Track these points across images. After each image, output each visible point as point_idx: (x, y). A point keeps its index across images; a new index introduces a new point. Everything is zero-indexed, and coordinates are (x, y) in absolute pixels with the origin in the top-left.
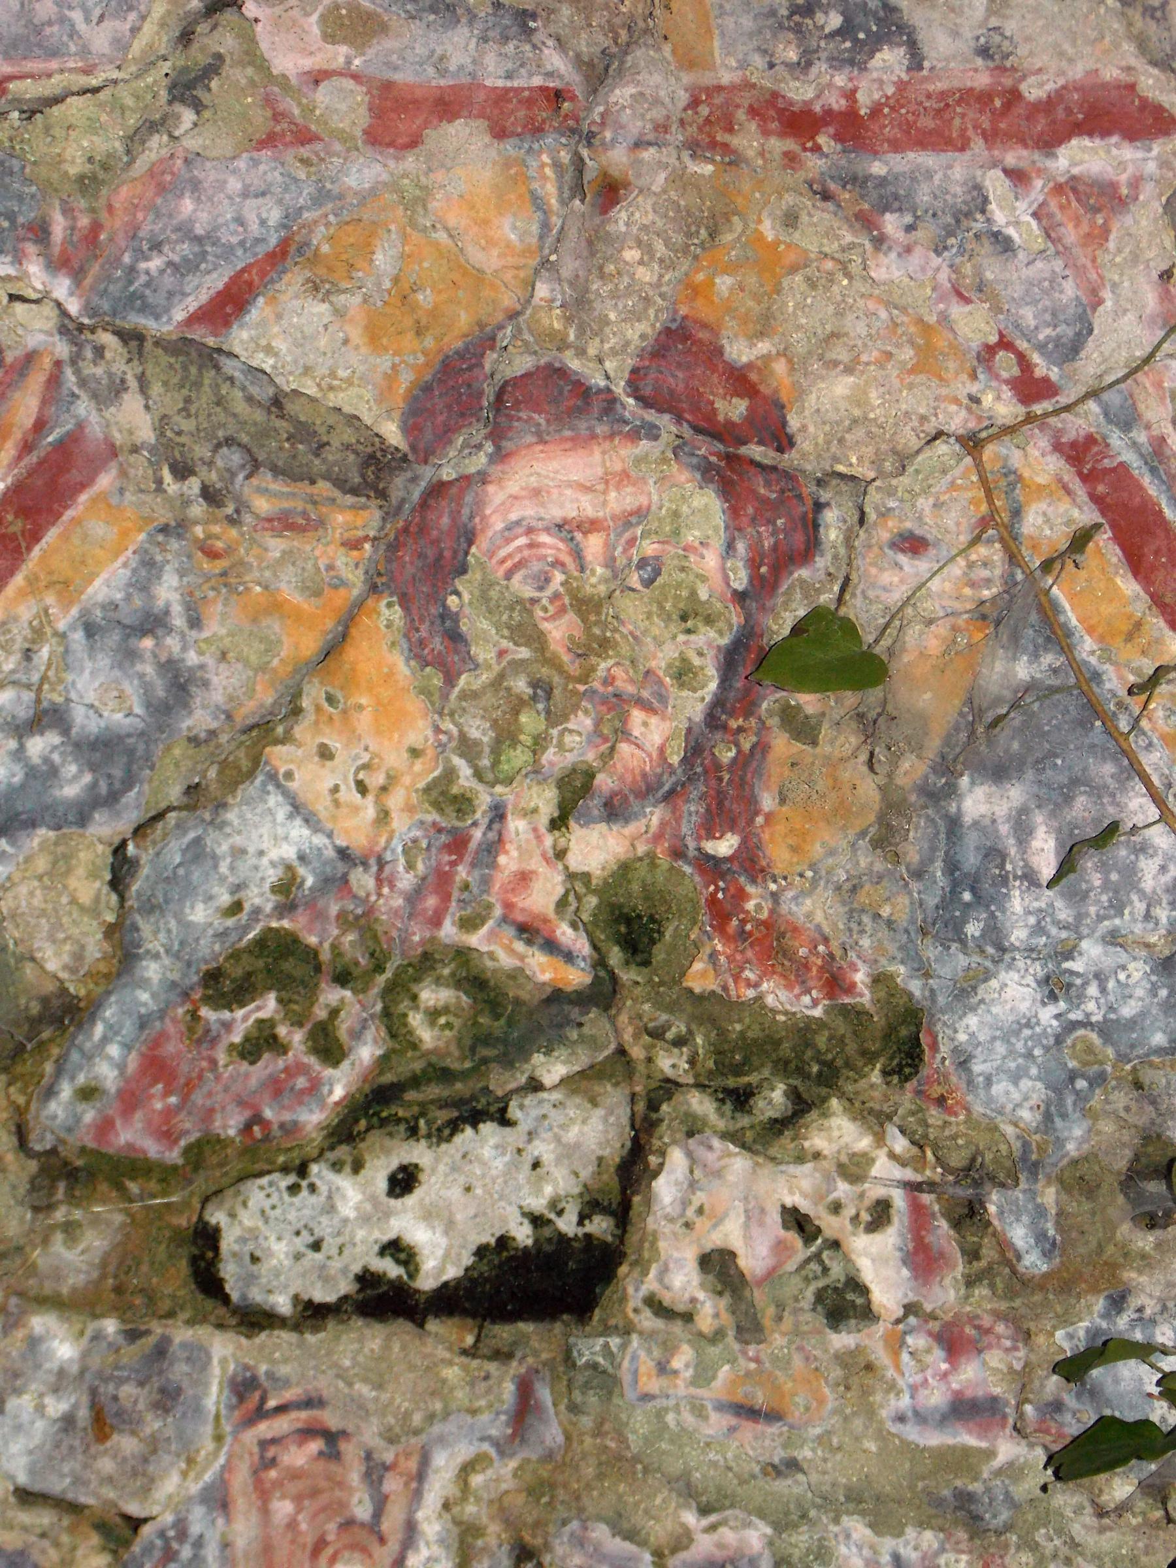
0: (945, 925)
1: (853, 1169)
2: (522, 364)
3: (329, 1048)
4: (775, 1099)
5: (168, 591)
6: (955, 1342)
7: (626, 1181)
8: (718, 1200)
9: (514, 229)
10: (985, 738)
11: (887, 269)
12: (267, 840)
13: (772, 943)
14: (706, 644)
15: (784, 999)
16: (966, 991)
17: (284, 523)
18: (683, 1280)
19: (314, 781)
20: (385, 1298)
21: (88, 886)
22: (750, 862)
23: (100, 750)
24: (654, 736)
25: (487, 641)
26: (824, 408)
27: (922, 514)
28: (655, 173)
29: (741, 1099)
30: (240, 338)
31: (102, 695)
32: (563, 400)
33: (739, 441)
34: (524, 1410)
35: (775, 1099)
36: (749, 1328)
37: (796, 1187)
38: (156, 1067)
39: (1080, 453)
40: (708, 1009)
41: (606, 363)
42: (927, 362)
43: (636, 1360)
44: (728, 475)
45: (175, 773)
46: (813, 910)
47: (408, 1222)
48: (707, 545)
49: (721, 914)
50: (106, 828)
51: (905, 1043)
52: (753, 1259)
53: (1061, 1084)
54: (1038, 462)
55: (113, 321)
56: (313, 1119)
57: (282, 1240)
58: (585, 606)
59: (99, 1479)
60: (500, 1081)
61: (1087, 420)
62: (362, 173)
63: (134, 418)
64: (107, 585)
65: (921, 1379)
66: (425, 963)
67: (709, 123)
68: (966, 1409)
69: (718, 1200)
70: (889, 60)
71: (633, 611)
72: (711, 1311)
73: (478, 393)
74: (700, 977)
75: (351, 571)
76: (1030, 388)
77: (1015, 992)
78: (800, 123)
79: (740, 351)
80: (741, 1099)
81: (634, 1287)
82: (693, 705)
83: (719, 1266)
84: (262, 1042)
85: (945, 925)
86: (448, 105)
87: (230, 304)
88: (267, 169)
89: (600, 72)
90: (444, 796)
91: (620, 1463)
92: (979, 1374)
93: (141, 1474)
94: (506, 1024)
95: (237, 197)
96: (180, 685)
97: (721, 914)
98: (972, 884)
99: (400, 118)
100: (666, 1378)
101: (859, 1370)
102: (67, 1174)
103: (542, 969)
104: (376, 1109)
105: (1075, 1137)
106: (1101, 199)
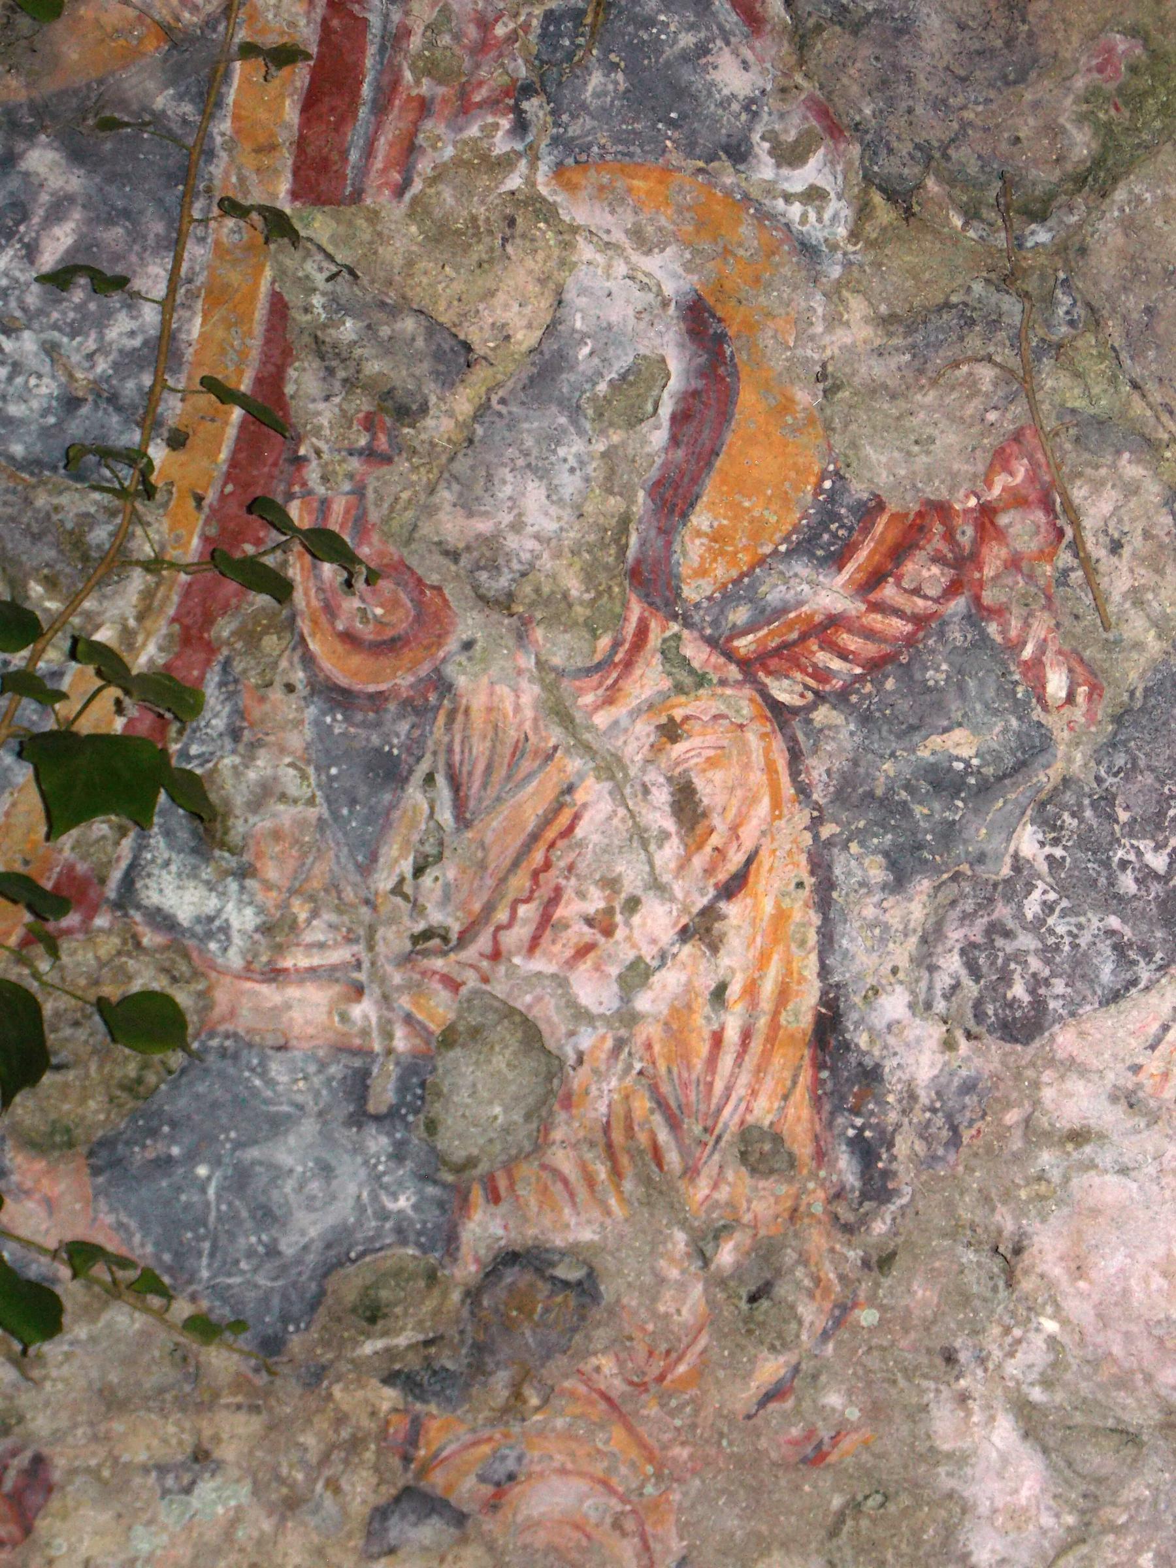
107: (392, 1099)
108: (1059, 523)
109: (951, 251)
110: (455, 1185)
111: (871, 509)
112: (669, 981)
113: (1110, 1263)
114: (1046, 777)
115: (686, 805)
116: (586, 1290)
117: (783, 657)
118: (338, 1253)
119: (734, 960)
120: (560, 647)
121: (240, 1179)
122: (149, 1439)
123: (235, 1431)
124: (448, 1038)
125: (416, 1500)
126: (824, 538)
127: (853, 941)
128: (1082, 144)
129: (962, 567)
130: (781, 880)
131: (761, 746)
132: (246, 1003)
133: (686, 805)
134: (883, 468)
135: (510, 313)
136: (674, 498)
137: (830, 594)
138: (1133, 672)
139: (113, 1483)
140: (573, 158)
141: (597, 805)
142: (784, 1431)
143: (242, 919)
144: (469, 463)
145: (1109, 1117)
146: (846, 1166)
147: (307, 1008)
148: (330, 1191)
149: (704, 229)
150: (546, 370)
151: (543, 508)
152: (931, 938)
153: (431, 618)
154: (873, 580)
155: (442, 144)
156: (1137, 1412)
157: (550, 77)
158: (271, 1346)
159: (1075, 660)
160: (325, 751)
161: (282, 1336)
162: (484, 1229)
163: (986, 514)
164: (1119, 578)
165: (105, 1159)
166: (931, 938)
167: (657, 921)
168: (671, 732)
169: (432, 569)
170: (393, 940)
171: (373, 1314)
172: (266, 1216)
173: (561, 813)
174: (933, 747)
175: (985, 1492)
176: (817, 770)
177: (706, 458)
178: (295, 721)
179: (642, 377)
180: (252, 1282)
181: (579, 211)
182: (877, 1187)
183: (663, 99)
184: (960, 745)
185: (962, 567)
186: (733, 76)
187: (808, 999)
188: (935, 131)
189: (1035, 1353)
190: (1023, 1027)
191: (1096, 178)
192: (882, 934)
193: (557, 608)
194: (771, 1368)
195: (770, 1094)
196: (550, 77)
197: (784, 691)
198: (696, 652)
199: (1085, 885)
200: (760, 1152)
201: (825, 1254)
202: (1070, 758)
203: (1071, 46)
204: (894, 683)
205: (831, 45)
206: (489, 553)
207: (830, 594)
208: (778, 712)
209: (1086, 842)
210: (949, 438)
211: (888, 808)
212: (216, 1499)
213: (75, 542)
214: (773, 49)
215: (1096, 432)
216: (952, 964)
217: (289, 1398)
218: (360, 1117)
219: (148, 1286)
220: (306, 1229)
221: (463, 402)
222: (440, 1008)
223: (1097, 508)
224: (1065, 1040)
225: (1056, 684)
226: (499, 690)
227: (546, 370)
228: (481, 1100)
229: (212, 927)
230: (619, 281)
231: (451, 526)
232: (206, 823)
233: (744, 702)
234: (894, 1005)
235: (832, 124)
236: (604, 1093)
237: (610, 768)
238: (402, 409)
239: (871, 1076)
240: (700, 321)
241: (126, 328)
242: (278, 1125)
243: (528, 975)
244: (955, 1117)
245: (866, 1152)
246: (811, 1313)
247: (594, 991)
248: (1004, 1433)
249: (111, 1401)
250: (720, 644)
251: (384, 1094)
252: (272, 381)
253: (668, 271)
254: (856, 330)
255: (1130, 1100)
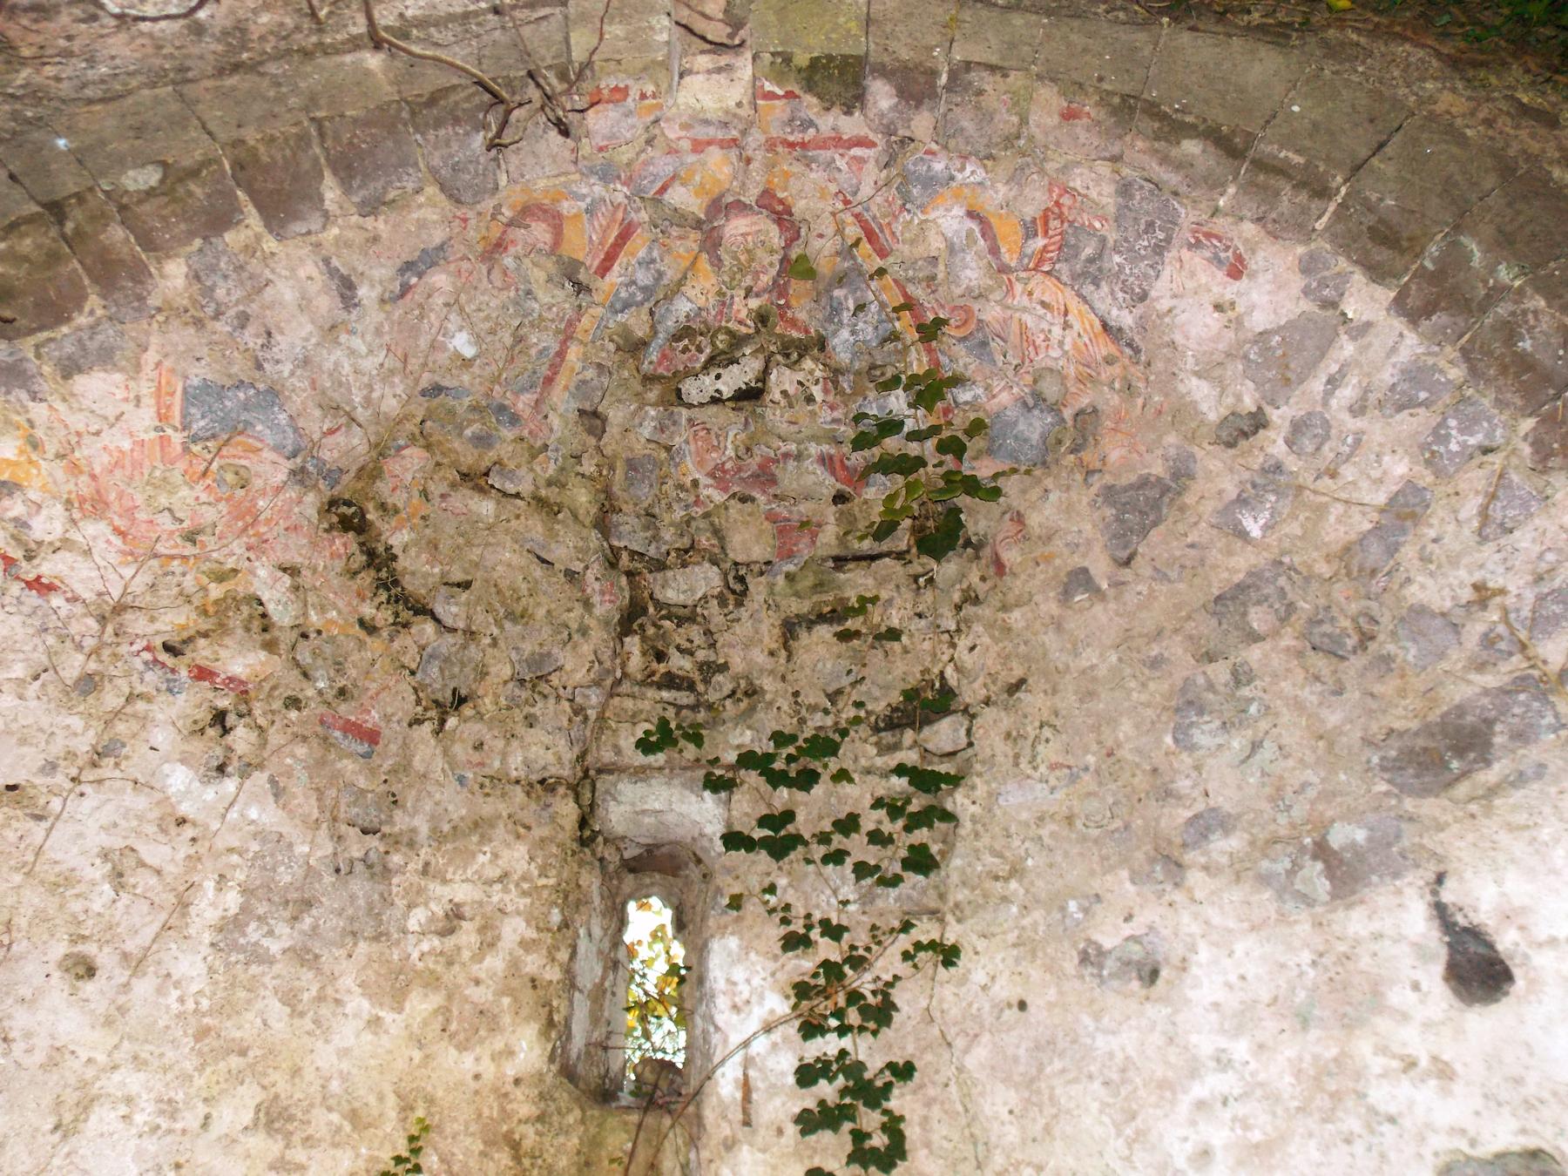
0: (830, 320)
1: (811, 372)
2: (730, 199)
3: (700, 350)
4: (795, 356)
5: (655, 254)
6: (832, 408)
7: (764, 376)
8: (783, 380)
9: (727, 170)
10: (840, 280)
11: (813, 175)
12: (682, 307)
13: (793, 323)
14: (777, 258)
15: (795, 334)
16: (835, 333)
17: (680, 238)
18: (777, 396)
19: (691, 293)
20: (716, 400)
21: (645, 317)
22: (788, 306)
23: (644, 289)
24: (766, 279)
25: (727, 260)
26: (799, 207)
27: (822, 229)
28: (759, 156)
29: (787, 356)
30: (666, 196)
31: (644, 278)
32: (740, 207)
33: (783, 216)
34: (746, 423)
35: (795, 356)
36: (791, 406)
37: (800, 376)
38: (664, 356)
39: (857, 216)
40: (781, 336)
41: (750, 198)
42: (822, 197)
43: (769, 412)
44: (779, 221)
45: (660, 294)
46: (802, 316)
47: (719, 385)
48: (775, 237)
49: (782, 317)
50: (647, 305)
51: (822, 343)
52: (791, 391)
53: (854, 354)
54: (850, 219)
55: (639, 193)
56: (698, 366)
57: (695, 389)
58: (748, 251)
59: (663, 439)
60: (738, 354)
61: (858, 210)
62: (691, 158)
63: (644, 216)
64: (642, 254)
65: (826, 415)
66: (719, 329)
67: (771, 145)
68: (834, 421)
69: (783, 380)
70: (812, 131)
71: (759, 253)
72: (783, 402)
73: (720, 207)
74: (778, 330)
75: (696, 247)
76: (846, 202)
77: (845, 334)
78: (792, 145)
79: (781, 195)
80: (787, 356)
81: (767, 398)
82: (774, 272)
83: (784, 393)
84: (685, 350)
85: (830, 320)
86: (709, 143)
87: (663, 189)
88: (669, 159)
89: (744, 133)
90: (720, 293)
91: (767, 432)
92: (837, 414)
93: (671, 438)
94: (737, 341)
95: (664, 166)
96: (660, 274)
97: (782, 317)
98: (836, 310)
99: (699, 146)
100: (775, 416)
101: (813, 414)
102: (649, 379)
103: (744, 330)
104: (711, 362)
105: (857, 365)
106: (861, 161)
107: (1036, 401)
108: (860, 751)
109: (1008, 161)
110: (1055, 409)
111: (1034, 221)
112: (1068, 340)
113: (1193, 332)
114: (1111, 243)
115: (1044, 304)
116: (1095, 411)
117: (1041, 261)
118: (1044, 438)
119: (1077, 326)
120: (997, 295)
121: (1016, 438)
122: (1035, 494)
123: (1049, 482)
124: (1035, 381)
125: (1090, 473)
126: (1030, 232)
127: (1097, 305)
128: (1015, 119)
129: (1061, 217)
130: (1074, 305)
131: (1050, 282)
132: (993, 406)
133: (1044, 304)
134: (1031, 211)
135: (936, 244)
136: (994, 251)
137: (1040, 242)
138: (1112, 210)
139: (1033, 506)
140: (923, 208)
141: (1029, 319)
142: (1150, 411)
143: (980, 391)
144: (952, 277)
145: (1174, 302)
146: (1128, 351)
147: (1004, 398)
148: (1034, 427)
149: (957, 196)
150: (951, 249)
151: (972, 273)
152: (1112, 293)
153: (967, 310)
154: (1046, 233)
155: (898, 228)
156: (1218, 357)
157: (906, 198)
158: (1044, 463)
159: (1098, 217)
160: (970, 350)
161: (1044, 459)
162: (1068, 414)
163: (1057, 204)
164: (1093, 194)
165: (990, 452)
166: (1112, 293)
167: (1057, 331)
168: (1030, 294)
169: (961, 302)
170: (1010, 373)
171: (1059, 442)
172: (1026, 440)
173: (1023, 328)
174: (1083, 256)
175: (1197, 396)
176: (1064, 278)
177: (994, 238)
178: (960, 350)
179: (970, 233)
180: (1032, 454)
181: (931, 216)
182: (1137, 351)
183: (929, 182)
184: (1089, 251)
185: (1061, 217)
186: (938, 166)
187: (1097, 323)
188: (985, 141)
189: (1191, 361)
190: (1143, 297)
191: (1024, 121)
192: (1102, 299)
193: (991, 289)
194: (1140, 401)
195: (1105, 348)
196: (906, 198)
197: (1046, 268)
198: (1023, 275)
199: (1135, 258)
200: (1109, 361)
201: (1136, 372)
202: (1112, 237)
203: (996, 104)
204: (1066, 249)
205: (952, 143)
206: (969, 289)
207: (1040, 242)
208: (1048, 273)
209: (1130, 250)
210: (1038, 194)
211: (1085, 274)
212: (1053, 497)
213: (897, 352)
214: (942, 155)
215: (1065, 169)
216: (1120, 295)
217: (1054, 469)
218: (1029, 410)
219: (1014, 471)
220: (1035, 437)
221: (941, 267)
222: (1029, 379)
223: (1077, 184)
224: (1153, 294)
225: (1097, 225)
226: (991, 313)
227: (951, 249)
228: (1050, 389)
229: (976, 397)
230: (950, 221)
231: (958, 291)
232: (957, 381)
233: (1039, 277)
234: (1115, 312)
235: (965, 158)
236: (1071, 371)
237: (1025, 310)
238: (933, 278)
239: (1120, 330)
240: (971, 214)
241: (874, 308)
242: (1016, 423)
243: (1041, 360)
244: (1142, 325)
245: (1129, 345)
246: (1141, 385)
247: (1055, 353)
248: (1194, 381)
249: (1024, 492)
250: (1027, 269)
251: (1031, 402)
252: (905, 295)
253: (958, 211)
254: (1002, 189)
255: (1175, 296)
